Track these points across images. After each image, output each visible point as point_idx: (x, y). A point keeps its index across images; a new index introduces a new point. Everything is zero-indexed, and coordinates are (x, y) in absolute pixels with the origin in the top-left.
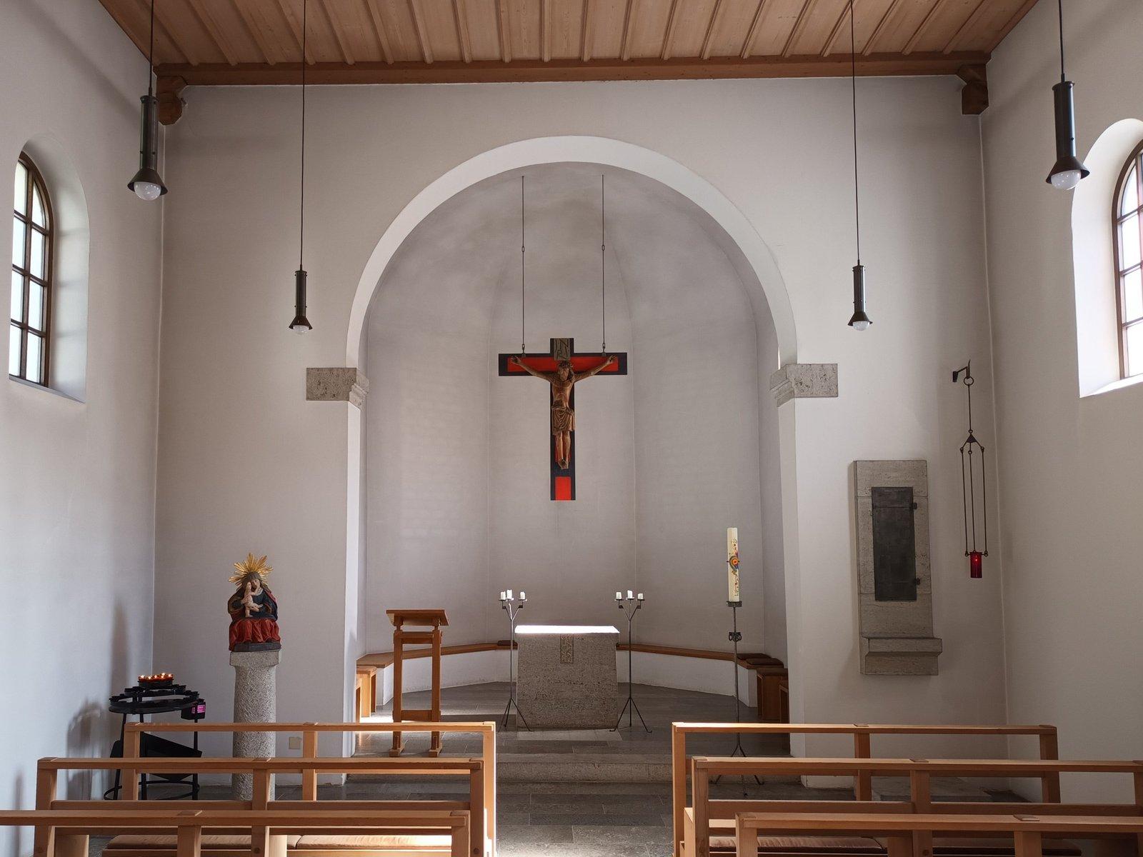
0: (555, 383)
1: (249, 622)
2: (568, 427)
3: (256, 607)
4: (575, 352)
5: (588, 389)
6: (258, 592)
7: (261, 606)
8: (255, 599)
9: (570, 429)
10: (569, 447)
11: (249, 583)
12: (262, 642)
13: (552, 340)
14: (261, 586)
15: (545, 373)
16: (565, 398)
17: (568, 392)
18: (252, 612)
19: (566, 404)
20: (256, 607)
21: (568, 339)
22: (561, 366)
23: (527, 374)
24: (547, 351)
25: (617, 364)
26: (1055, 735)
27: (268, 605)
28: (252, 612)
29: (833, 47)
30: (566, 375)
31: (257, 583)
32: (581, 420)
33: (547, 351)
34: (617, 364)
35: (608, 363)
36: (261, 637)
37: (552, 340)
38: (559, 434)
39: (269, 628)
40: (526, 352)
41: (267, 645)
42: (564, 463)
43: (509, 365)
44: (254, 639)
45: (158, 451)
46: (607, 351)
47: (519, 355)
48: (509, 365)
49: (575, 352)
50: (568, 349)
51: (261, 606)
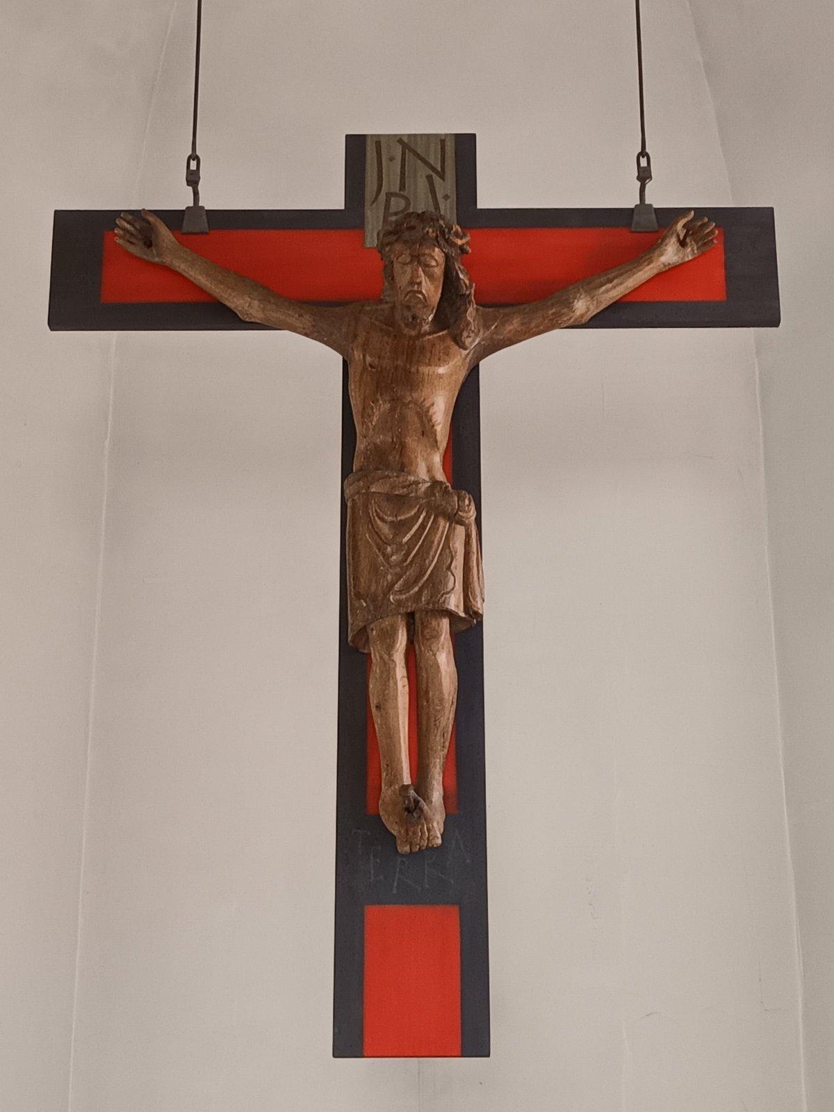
0: (365, 348)
2: (436, 585)
4: (483, 202)
5: (539, 380)
9: (454, 602)
10: (447, 717)
13: (356, 146)
15: (319, 309)
16: (427, 430)
17: (440, 408)
19: (429, 465)
21: (442, 140)
22: (406, 278)
23: (219, 316)
24: (333, 198)
25: (726, 270)
26: (102, 221)
30: (431, 290)
32: (536, 566)
33: (333, 198)
34: (726, 270)
35: (670, 254)
37: (356, 146)
38: (388, 637)
40: (212, 200)
42: (413, 811)
43: (113, 272)
45: (785, 774)
46: (658, 197)
47: (172, 218)
48: (113, 272)
49: (483, 202)
50: (446, 187)
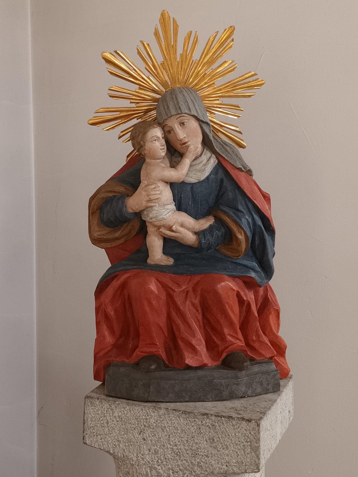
1: (153, 287)
3: (187, 227)
4: (133, 149)
6: (198, 168)
7: (206, 223)
8: (185, 197)
11: (157, 132)
12: (202, 367)
14: (206, 143)
18: (171, 244)
20: (187, 227)
27: (235, 221)
28: (171, 244)
29: (105, 386)
31: (189, 134)
36: (202, 348)
39: (234, 313)
41: (222, 377)
44: (173, 356)
49: (133, 149)
51: (206, 223)
